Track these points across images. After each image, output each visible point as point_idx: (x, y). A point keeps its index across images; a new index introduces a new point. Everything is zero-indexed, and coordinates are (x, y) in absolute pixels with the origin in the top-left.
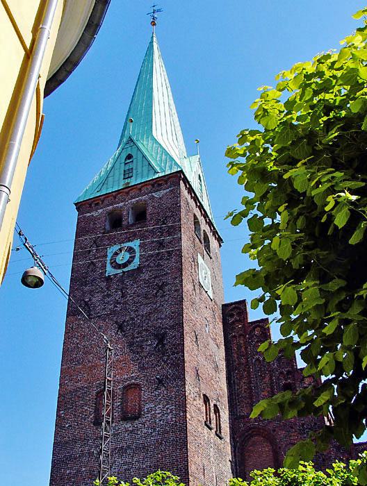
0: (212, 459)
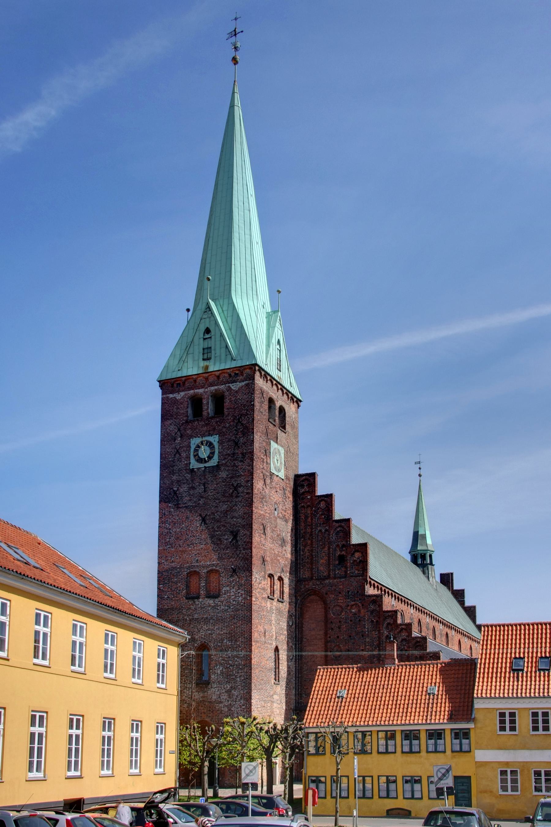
0: (273, 622)
